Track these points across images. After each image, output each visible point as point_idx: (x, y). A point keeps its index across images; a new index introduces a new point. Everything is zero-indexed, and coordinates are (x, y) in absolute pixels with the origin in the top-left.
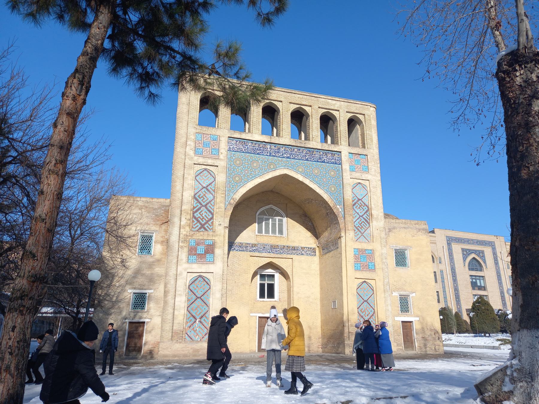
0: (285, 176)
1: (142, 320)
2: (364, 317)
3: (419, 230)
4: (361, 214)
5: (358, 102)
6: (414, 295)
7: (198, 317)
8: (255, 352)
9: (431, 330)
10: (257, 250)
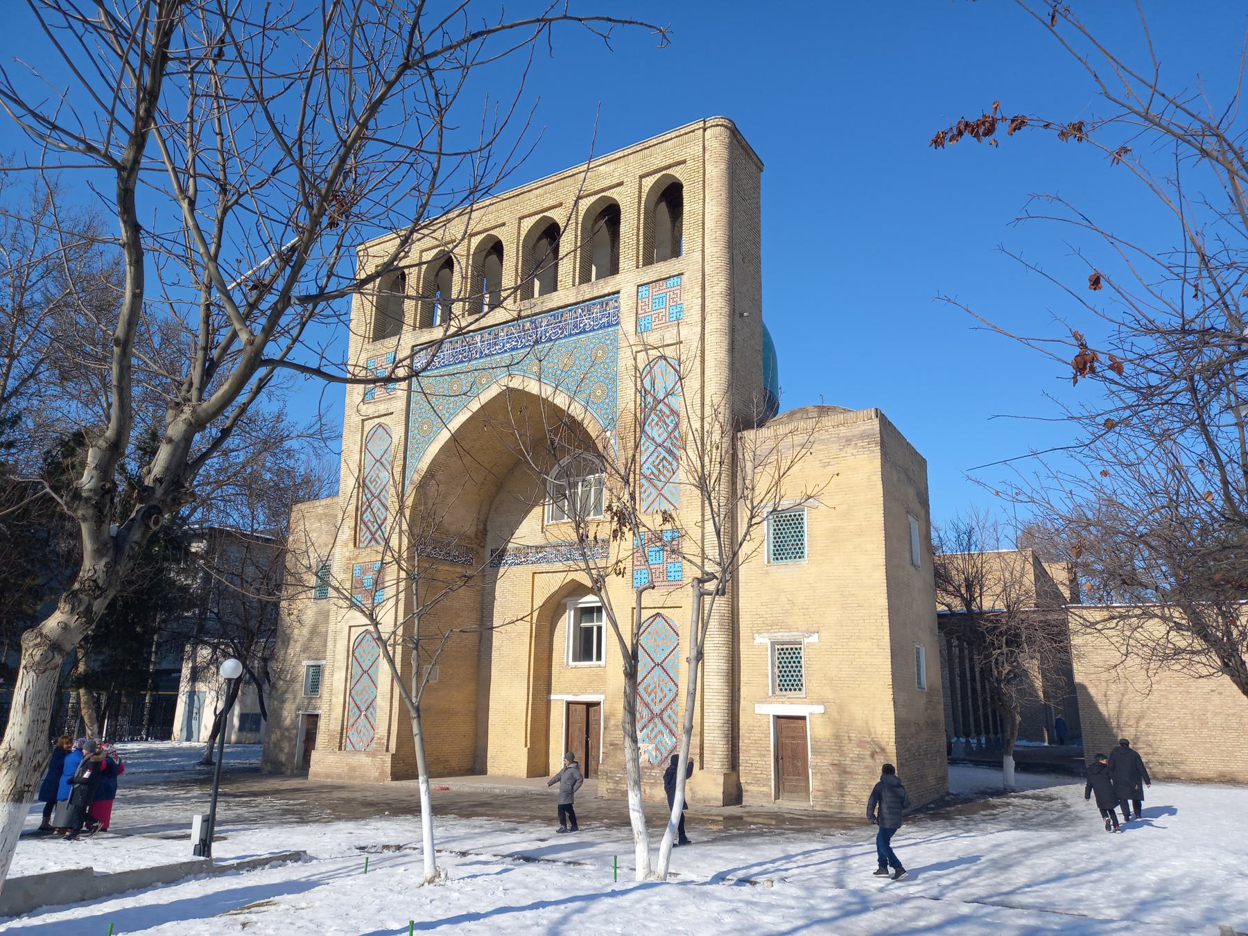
0: (511, 394)
1: (316, 712)
2: (652, 706)
3: (849, 441)
4: (659, 440)
5: (668, 136)
6: (814, 639)
7: (363, 709)
8: (521, 779)
9: (861, 744)
10: (544, 558)
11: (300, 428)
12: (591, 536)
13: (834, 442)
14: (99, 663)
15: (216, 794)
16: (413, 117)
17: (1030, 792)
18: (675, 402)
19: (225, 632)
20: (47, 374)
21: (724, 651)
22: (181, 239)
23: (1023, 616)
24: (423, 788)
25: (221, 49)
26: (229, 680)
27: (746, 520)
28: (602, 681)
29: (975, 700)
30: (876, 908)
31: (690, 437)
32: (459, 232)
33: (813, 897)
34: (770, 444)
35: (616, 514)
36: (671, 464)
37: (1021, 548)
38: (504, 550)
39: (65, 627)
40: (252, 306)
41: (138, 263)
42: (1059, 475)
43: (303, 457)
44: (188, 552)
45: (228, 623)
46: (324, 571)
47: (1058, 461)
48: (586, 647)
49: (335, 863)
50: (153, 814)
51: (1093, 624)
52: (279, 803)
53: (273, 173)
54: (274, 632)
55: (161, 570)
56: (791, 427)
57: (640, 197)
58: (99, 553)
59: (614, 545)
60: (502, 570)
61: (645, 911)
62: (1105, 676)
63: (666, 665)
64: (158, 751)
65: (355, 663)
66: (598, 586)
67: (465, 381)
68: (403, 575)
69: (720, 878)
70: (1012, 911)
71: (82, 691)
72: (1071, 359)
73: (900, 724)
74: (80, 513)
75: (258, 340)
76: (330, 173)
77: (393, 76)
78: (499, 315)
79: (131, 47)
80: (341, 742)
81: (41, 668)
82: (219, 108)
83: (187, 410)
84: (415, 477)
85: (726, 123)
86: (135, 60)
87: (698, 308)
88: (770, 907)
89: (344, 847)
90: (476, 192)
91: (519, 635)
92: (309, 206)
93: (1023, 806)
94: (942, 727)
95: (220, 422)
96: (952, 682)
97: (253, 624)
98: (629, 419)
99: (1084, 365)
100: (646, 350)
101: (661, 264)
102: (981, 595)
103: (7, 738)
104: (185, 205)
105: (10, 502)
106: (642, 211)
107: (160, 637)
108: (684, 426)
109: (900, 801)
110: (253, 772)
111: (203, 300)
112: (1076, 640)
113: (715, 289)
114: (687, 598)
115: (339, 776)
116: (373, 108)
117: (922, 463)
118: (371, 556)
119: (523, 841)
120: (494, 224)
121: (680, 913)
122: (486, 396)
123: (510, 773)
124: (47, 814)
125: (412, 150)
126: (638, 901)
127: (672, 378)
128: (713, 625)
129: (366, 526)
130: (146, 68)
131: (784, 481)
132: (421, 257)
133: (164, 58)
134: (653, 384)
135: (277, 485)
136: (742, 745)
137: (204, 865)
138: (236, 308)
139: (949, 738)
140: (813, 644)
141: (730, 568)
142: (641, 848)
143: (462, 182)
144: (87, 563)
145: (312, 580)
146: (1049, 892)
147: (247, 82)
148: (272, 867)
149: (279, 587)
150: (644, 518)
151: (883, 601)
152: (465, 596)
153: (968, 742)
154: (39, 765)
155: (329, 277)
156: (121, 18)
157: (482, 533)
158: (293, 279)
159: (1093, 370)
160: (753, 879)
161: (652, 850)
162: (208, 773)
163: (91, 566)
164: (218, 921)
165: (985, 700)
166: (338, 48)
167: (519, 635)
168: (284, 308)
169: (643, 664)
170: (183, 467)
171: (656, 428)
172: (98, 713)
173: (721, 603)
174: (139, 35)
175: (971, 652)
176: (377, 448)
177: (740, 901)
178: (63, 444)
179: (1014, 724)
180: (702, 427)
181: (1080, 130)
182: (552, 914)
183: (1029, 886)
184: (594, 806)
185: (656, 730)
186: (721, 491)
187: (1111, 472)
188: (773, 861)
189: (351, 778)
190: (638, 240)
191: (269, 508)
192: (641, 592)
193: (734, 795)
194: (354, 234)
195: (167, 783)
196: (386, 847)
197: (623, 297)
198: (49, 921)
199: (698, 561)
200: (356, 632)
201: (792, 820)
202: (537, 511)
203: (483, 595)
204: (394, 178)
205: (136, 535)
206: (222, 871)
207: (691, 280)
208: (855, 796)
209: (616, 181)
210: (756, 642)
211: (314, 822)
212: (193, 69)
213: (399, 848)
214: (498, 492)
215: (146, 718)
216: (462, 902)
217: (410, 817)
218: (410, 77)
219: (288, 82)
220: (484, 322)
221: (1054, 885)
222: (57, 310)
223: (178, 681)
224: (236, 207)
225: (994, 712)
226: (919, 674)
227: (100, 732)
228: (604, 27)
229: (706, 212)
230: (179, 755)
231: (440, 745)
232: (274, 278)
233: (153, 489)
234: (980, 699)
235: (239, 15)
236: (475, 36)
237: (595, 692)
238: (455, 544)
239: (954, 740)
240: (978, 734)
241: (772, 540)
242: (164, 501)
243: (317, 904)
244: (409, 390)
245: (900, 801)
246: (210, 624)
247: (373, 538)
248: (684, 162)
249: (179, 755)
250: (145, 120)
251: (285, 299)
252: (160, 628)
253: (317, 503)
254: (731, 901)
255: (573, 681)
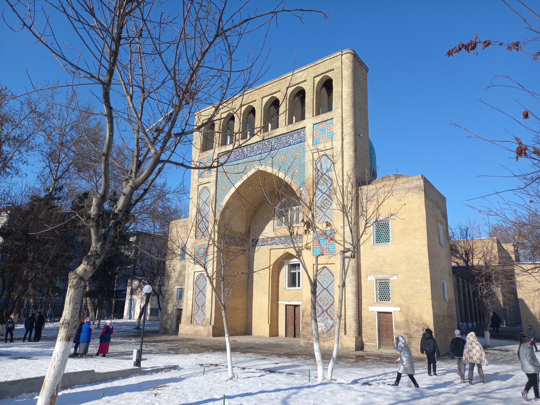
0: (260, 173)
2: (323, 306)
3: (409, 189)
4: (324, 191)
5: (326, 59)
6: (395, 278)
8: (266, 337)
9: (417, 325)
11: (172, 189)
12: (295, 234)
13: (402, 190)
14: (95, 287)
15: (142, 342)
16: (219, 57)
17: (497, 348)
18: (332, 174)
19: (144, 274)
20: (73, 169)
21: (354, 283)
22: (126, 112)
23: (493, 268)
24: (227, 339)
25: (141, 33)
26: (147, 294)
27: (363, 225)
28: (301, 296)
29: (470, 306)
30: (427, 397)
31: (338, 189)
32: (237, 105)
33: (398, 391)
34: (374, 191)
35: (306, 223)
36: (329, 201)
37: (490, 235)
38: (258, 239)
39: (85, 270)
40: (156, 138)
41: (111, 122)
42: (510, 203)
43: (174, 201)
44: (129, 242)
45: (145, 271)
46: (184, 249)
47: (509, 196)
48: (293, 281)
49: (191, 371)
50: (117, 349)
51: (527, 271)
52: (167, 345)
53: (163, 83)
54: (163, 274)
55: (118, 249)
56: (383, 184)
57: (314, 86)
58: (98, 240)
59: (305, 237)
60: (257, 248)
61: (323, 394)
62: (532, 294)
63: (328, 289)
64: (118, 323)
65: (197, 287)
66: (299, 254)
67: (241, 168)
68: (216, 249)
69: (355, 382)
70: (490, 400)
71: (88, 299)
72: (515, 149)
73: (435, 316)
74: (90, 224)
75: (158, 153)
76: (187, 82)
77: (212, 40)
78: (256, 139)
79: (107, 35)
80: (191, 321)
81: (76, 287)
82: (141, 57)
83: (131, 182)
84: (220, 209)
85: (351, 52)
86: (109, 40)
87: (340, 133)
88: (379, 395)
89: (194, 364)
90: (246, 86)
91: (265, 276)
92: (178, 96)
93: (494, 354)
94: (455, 317)
95: (143, 187)
96: (459, 297)
97: (155, 271)
98: (311, 181)
99: (521, 152)
100: (318, 152)
101: (324, 114)
102: (472, 258)
103: (63, 315)
104: (129, 98)
105: (59, 222)
106: (315, 92)
107: (118, 276)
108: (335, 184)
109: (439, 347)
110: (156, 333)
111: (136, 137)
112: (518, 279)
113: (348, 124)
114: (337, 260)
115: (191, 335)
116: (203, 54)
117: (444, 199)
118: (204, 242)
119: (269, 363)
120: (251, 100)
121: (338, 396)
122: (250, 173)
123: (262, 335)
124: (76, 348)
125: (219, 70)
126: (320, 390)
127: (329, 163)
128: (349, 272)
129: (199, 229)
130: (113, 42)
131: (381, 207)
132: (221, 116)
133: (120, 38)
134: (321, 167)
135: (163, 213)
136: (364, 324)
137: (138, 371)
138: (149, 139)
139: (458, 323)
140: (395, 280)
141: (356, 246)
142: (320, 368)
143: (240, 83)
144: (93, 244)
145: (179, 252)
146: (508, 393)
147: (153, 46)
148: (165, 372)
149: (165, 255)
150: (318, 225)
151: (427, 261)
152: (241, 259)
153: (467, 325)
154: (76, 326)
155: (186, 125)
156: (103, 23)
157: (248, 232)
158: (172, 127)
159: (525, 154)
160: (370, 383)
161: (325, 369)
162: (138, 333)
163: (95, 246)
164: (145, 393)
165: (475, 306)
166: (189, 30)
167: (265, 276)
168: (169, 139)
169: (319, 289)
170: (129, 205)
171: (322, 186)
172: (94, 307)
173: (353, 261)
174: (110, 29)
175: (468, 284)
176: (204, 197)
177: (365, 391)
178: (80, 198)
179: (489, 317)
180: (343, 185)
181: (517, 45)
182: (283, 395)
183: (498, 390)
184: (298, 349)
185: (325, 317)
186: (352, 213)
187: (535, 201)
188: (379, 376)
189: (195, 335)
190: (313, 105)
191: (161, 223)
192: (318, 257)
193: (360, 346)
194: (196, 107)
195: (122, 336)
196: (211, 365)
197: (307, 130)
198: (78, 391)
199: (342, 243)
200: (197, 274)
201: (387, 358)
202: (271, 222)
203: (249, 259)
204: (211, 83)
205: (112, 233)
206: (145, 373)
207: (337, 121)
208: (415, 348)
209: (303, 80)
210: (369, 279)
211: (181, 354)
212: (131, 42)
213: (216, 365)
214: (254, 215)
215: (113, 310)
216: (244, 388)
217: (220, 352)
218: (218, 40)
219: (168, 45)
220: (247, 143)
221: (510, 390)
222: (76, 143)
223: (125, 294)
224: (148, 98)
225: (479, 311)
226: (444, 294)
227: (95, 315)
228: (299, 13)
229: (343, 91)
230: (127, 325)
231: (232, 321)
232: (164, 126)
233: (118, 214)
234: (473, 306)
235: (148, 19)
236: (245, 21)
237: (298, 301)
238: (237, 238)
239: (461, 324)
240: (472, 321)
241: (375, 234)
242: (122, 219)
243: (185, 387)
244: (217, 171)
245: (439, 347)
246: (137, 271)
247: (203, 235)
248: (333, 70)
249: (127, 325)
250: (113, 64)
251: (169, 135)
252: (118, 273)
253: (180, 220)
254: (361, 391)
255: (288, 296)
